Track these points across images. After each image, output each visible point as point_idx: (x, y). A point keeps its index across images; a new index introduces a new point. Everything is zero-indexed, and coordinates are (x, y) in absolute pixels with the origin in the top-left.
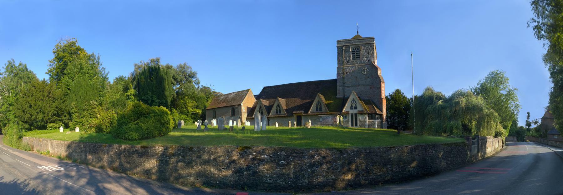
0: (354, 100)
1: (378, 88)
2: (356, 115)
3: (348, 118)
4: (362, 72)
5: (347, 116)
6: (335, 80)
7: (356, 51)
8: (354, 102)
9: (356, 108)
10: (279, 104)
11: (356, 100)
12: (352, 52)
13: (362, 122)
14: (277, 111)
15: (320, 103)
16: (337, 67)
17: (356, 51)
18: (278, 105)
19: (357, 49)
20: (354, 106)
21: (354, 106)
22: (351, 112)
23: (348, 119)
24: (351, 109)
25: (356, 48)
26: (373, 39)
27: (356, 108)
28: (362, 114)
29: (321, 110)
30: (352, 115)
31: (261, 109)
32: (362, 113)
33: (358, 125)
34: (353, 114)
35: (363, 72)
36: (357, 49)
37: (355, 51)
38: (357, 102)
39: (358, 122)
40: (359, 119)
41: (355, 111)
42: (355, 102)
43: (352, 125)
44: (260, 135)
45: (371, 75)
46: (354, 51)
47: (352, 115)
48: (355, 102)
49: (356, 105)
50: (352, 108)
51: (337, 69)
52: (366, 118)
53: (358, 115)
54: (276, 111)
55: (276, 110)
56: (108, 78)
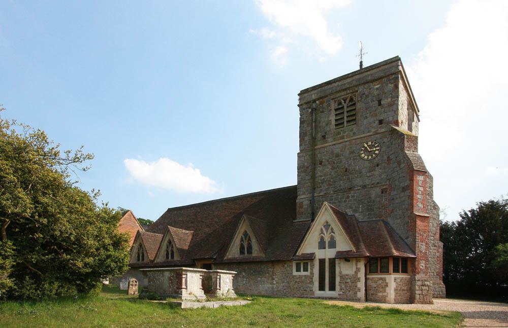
0: (327, 226)
1: (403, 188)
2: (332, 262)
3: (312, 269)
4: (359, 155)
5: (309, 264)
6: (282, 198)
7: (345, 105)
8: (327, 230)
9: (333, 244)
10: (171, 239)
11: (333, 225)
12: (336, 110)
13: (349, 280)
14: (168, 254)
15: (250, 237)
16: (298, 154)
17: (345, 105)
18: (170, 242)
19: (347, 101)
20: (327, 239)
21: (327, 239)
22: (320, 254)
23: (312, 273)
24: (320, 248)
25: (345, 101)
26: (396, 60)
27: (333, 244)
28: (347, 260)
29: (251, 253)
30: (322, 262)
31: (141, 250)
32: (345, 257)
33: (337, 287)
34: (325, 259)
35: (363, 155)
36: (347, 101)
37: (343, 108)
38: (335, 230)
39: (338, 280)
40: (340, 272)
41: (329, 254)
42: (330, 231)
43: (322, 288)
44: (218, 270)
45: (385, 157)
46: (340, 106)
47: (322, 262)
48: (330, 231)
49: (332, 238)
50: (322, 245)
51: (298, 157)
52: (358, 270)
53: (337, 261)
54: (166, 254)
55: (165, 253)
56: (360, 278)
